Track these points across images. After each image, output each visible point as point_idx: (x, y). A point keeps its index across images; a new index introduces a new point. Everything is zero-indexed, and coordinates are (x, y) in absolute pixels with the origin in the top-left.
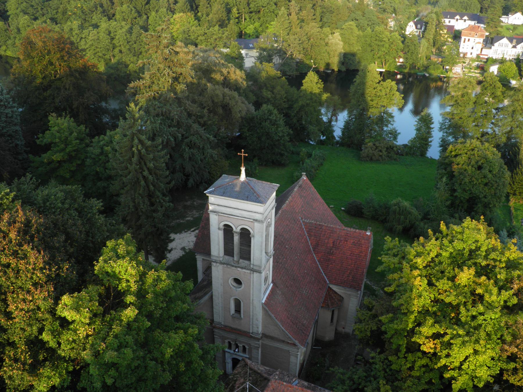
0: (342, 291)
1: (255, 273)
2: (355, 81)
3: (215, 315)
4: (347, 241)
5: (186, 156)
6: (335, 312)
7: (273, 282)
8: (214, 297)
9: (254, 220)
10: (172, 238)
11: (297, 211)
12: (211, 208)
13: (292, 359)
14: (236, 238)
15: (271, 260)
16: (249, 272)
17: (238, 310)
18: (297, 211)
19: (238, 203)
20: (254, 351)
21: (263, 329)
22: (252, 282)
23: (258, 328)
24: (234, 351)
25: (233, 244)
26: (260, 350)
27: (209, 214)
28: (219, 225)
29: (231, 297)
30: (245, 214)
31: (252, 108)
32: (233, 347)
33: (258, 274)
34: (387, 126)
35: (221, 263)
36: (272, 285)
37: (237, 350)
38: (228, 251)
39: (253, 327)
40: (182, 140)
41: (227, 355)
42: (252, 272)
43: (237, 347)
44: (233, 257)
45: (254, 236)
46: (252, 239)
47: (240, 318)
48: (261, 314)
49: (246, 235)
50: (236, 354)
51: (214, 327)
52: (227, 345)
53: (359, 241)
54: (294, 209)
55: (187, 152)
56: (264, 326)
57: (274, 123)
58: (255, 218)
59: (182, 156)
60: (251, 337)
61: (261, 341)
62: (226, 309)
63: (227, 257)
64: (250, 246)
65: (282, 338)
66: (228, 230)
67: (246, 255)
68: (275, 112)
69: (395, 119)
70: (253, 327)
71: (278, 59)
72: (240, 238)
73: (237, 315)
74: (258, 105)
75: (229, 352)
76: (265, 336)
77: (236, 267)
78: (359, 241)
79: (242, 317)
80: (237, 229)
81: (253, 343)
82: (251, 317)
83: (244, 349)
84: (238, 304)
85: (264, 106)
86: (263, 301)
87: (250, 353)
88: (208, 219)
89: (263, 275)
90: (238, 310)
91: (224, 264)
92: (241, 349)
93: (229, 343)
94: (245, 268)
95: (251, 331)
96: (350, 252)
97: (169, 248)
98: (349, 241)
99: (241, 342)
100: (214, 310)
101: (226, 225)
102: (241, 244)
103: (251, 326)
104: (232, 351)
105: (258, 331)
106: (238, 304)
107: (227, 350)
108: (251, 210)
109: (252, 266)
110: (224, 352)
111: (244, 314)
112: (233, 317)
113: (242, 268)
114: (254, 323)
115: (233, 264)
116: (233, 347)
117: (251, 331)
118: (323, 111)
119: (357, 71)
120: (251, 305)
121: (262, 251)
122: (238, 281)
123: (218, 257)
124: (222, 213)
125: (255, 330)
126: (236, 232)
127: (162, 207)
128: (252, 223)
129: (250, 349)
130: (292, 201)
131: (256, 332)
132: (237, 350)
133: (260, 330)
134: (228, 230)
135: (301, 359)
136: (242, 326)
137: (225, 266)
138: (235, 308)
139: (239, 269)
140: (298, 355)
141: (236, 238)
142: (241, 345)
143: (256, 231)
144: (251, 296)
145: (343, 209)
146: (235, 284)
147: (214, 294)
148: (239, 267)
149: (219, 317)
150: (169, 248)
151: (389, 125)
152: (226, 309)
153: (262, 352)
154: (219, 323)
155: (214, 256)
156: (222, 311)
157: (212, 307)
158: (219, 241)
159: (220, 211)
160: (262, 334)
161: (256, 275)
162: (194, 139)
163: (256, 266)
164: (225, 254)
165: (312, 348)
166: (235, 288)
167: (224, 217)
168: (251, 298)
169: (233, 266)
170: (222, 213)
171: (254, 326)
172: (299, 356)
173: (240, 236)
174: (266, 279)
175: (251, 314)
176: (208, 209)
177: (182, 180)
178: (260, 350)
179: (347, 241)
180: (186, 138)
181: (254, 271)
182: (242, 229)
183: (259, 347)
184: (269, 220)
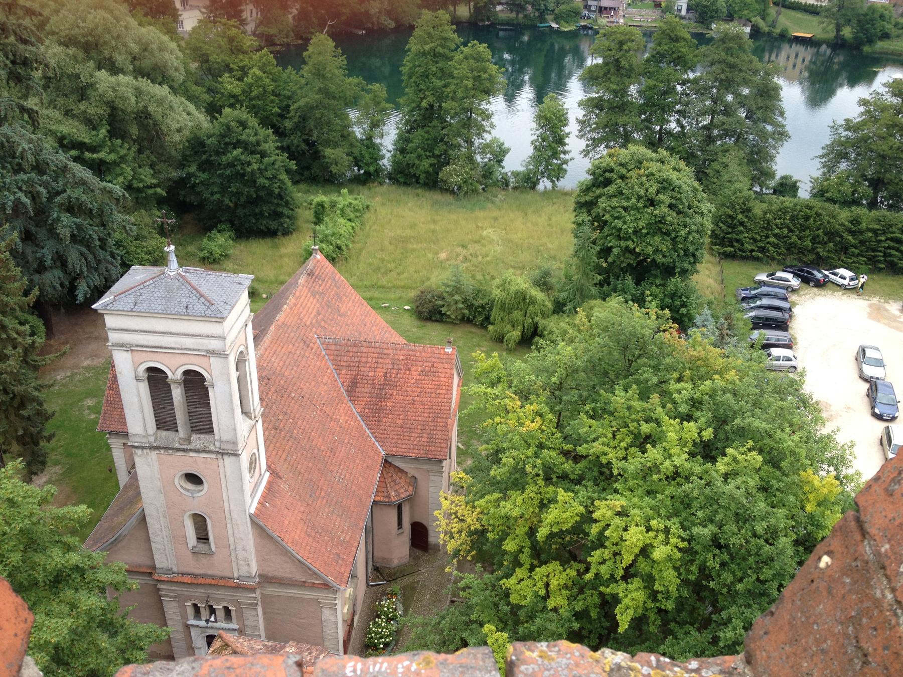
0: (409, 466)
1: (226, 457)
2: (409, 50)
3: (156, 556)
4: (410, 370)
5: (64, 232)
6: (403, 508)
7: (269, 468)
8: (148, 520)
9: (208, 351)
10: (50, 412)
11: (308, 323)
12: (113, 337)
13: (327, 615)
14: (177, 393)
15: (260, 426)
16: (214, 456)
17: (203, 537)
18: (308, 323)
19: (170, 321)
20: (248, 614)
21: (259, 566)
22: (222, 476)
23: (249, 565)
24: (207, 621)
25: (172, 404)
26: (260, 609)
27: (110, 351)
28: (135, 371)
29: (185, 512)
30: (188, 342)
31: (201, 117)
32: (204, 613)
33: (232, 458)
34: (479, 135)
35: (152, 448)
36: (268, 474)
37: (212, 619)
38: (165, 421)
39: (238, 565)
40: (50, 199)
41: (193, 632)
42: (220, 456)
43: (212, 611)
44: (177, 431)
45: (212, 386)
46: (210, 389)
47: (211, 554)
48: (251, 536)
49: (195, 383)
50: (212, 628)
51: (158, 580)
52: (190, 611)
53: (433, 366)
54: (301, 320)
55: (66, 223)
56: (262, 560)
57: (251, 148)
58: (211, 347)
59: (52, 233)
60: (238, 587)
61: (258, 591)
62: (178, 538)
63: (164, 434)
64: (208, 404)
65: (300, 577)
66: (156, 379)
67: (202, 422)
68: (253, 122)
69: (495, 120)
70: (238, 565)
71: (254, 11)
72: (186, 391)
73: (202, 547)
74: (213, 110)
75: (197, 626)
76: (266, 579)
77: (185, 450)
78: (433, 366)
79: (213, 549)
80: (174, 374)
81: (244, 598)
82: (232, 547)
83: (227, 612)
84: (200, 522)
85: (227, 110)
86: (252, 511)
87: (241, 618)
88: (110, 365)
89: (245, 459)
90: (203, 537)
91: (157, 448)
92: (220, 614)
93: (195, 606)
94: (204, 451)
95: (236, 575)
96: (419, 390)
97: (46, 434)
98: (413, 368)
99: (219, 601)
100: (153, 545)
101: (151, 370)
102: (189, 402)
103: (234, 565)
104: (202, 623)
105: (250, 573)
106: (200, 522)
107: (192, 622)
108: (198, 333)
109: (217, 444)
110: (188, 627)
111: (215, 544)
112: (195, 553)
113: (198, 451)
114: (240, 557)
115: (177, 445)
116: (204, 613)
117: (236, 575)
118: (353, 114)
119: (412, 28)
120: (228, 521)
121: (233, 411)
122: (194, 479)
123: (143, 436)
124: (137, 346)
125: (244, 571)
126: (175, 382)
127: (15, 348)
128: (206, 359)
129: (240, 611)
130: (295, 305)
131: (246, 574)
132: (212, 619)
133: (254, 569)
134: (156, 379)
135: (345, 611)
136: (217, 566)
137: (162, 452)
138: (197, 533)
139: (191, 454)
140: (336, 604)
141: (177, 393)
142: (218, 607)
143: (215, 373)
144: (226, 504)
145: (407, 307)
146: (189, 486)
147: (146, 512)
148: (191, 450)
149: (165, 557)
150: (46, 434)
151: (486, 135)
152: (178, 538)
153: (264, 613)
154: (169, 571)
155: (137, 435)
156: (170, 548)
157: (148, 540)
158: (141, 407)
159: (135, 343)
160: (261, 576)
161: (228, 460)
162: (76, 193)
163: (226, 442)
164: (158, 428)
165: (368, 585)
166: (189, 494)
167: (144, 354)
168: (227, 509)
169: (178, 450)
170: (137, 346)
171: (241, 562)
172: (339, 607)
173: (185, 387)
174: (253, 464)
175: (231, 539)
176: (107, 339)
177: (61, 285)
178: (260, 609)
179: (410, 370)
180: (58, 193)
181: (223, 454)
182: (187, 373)
183: (256, 604)
184: (242, 348)
